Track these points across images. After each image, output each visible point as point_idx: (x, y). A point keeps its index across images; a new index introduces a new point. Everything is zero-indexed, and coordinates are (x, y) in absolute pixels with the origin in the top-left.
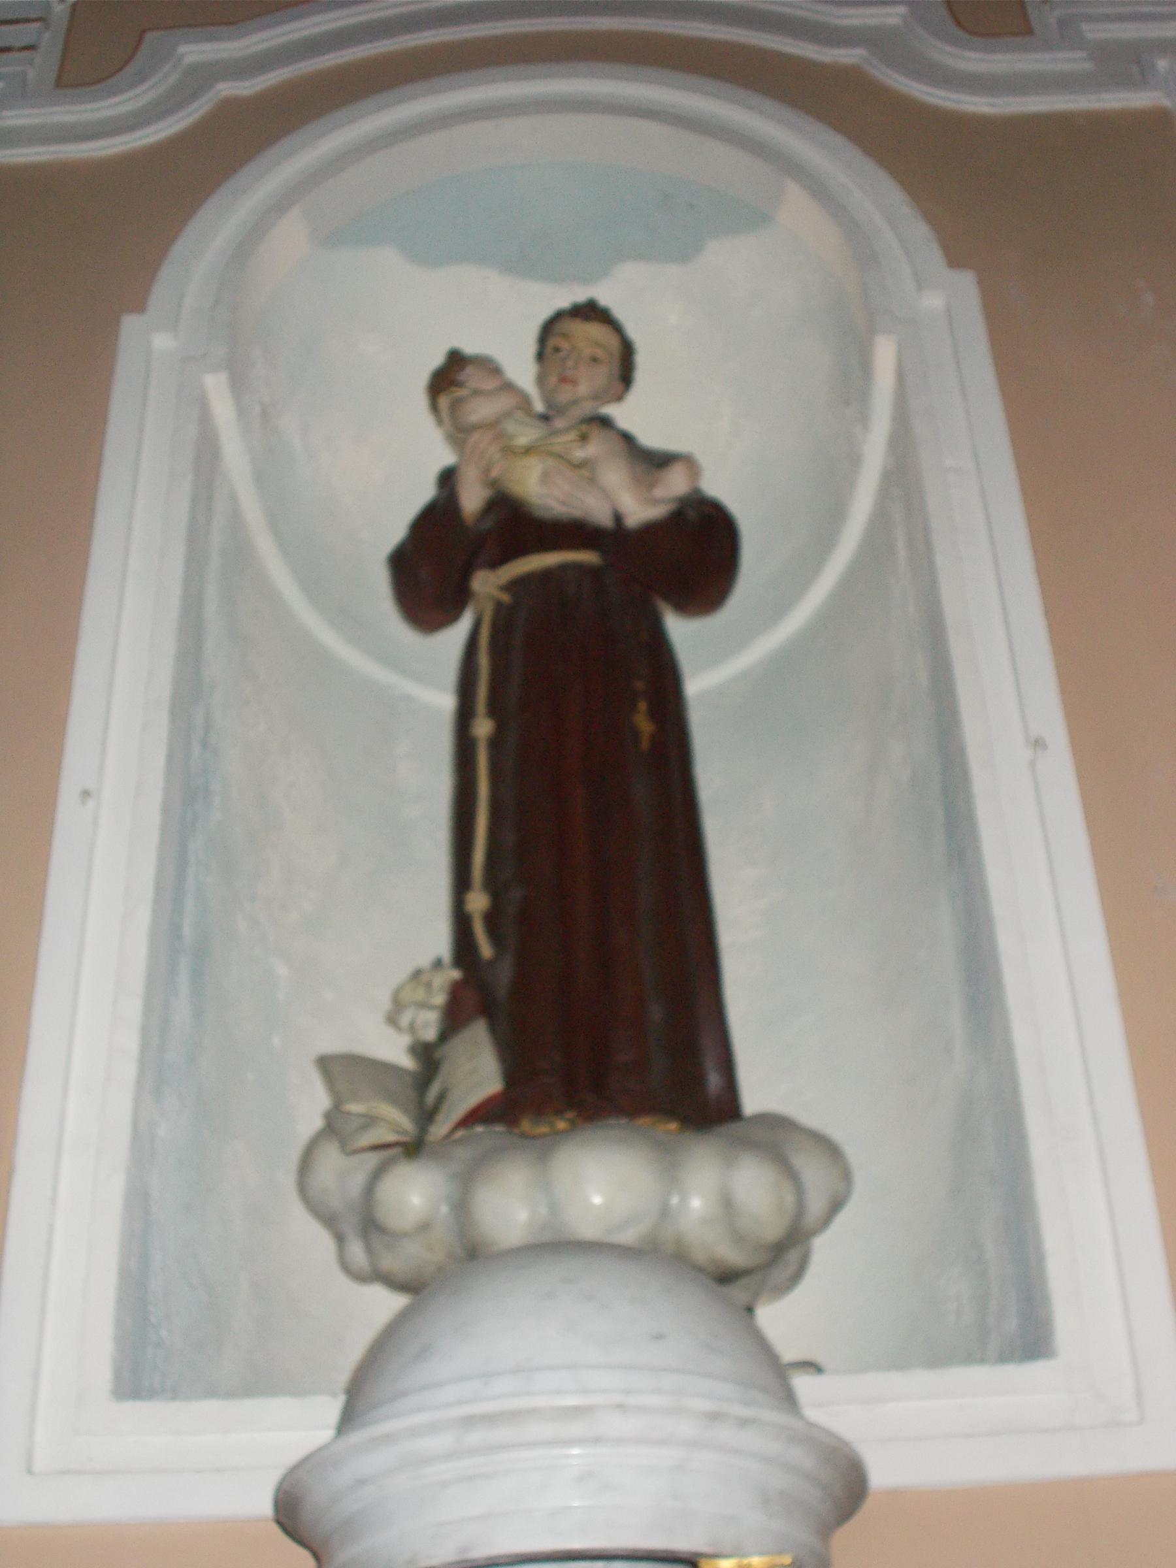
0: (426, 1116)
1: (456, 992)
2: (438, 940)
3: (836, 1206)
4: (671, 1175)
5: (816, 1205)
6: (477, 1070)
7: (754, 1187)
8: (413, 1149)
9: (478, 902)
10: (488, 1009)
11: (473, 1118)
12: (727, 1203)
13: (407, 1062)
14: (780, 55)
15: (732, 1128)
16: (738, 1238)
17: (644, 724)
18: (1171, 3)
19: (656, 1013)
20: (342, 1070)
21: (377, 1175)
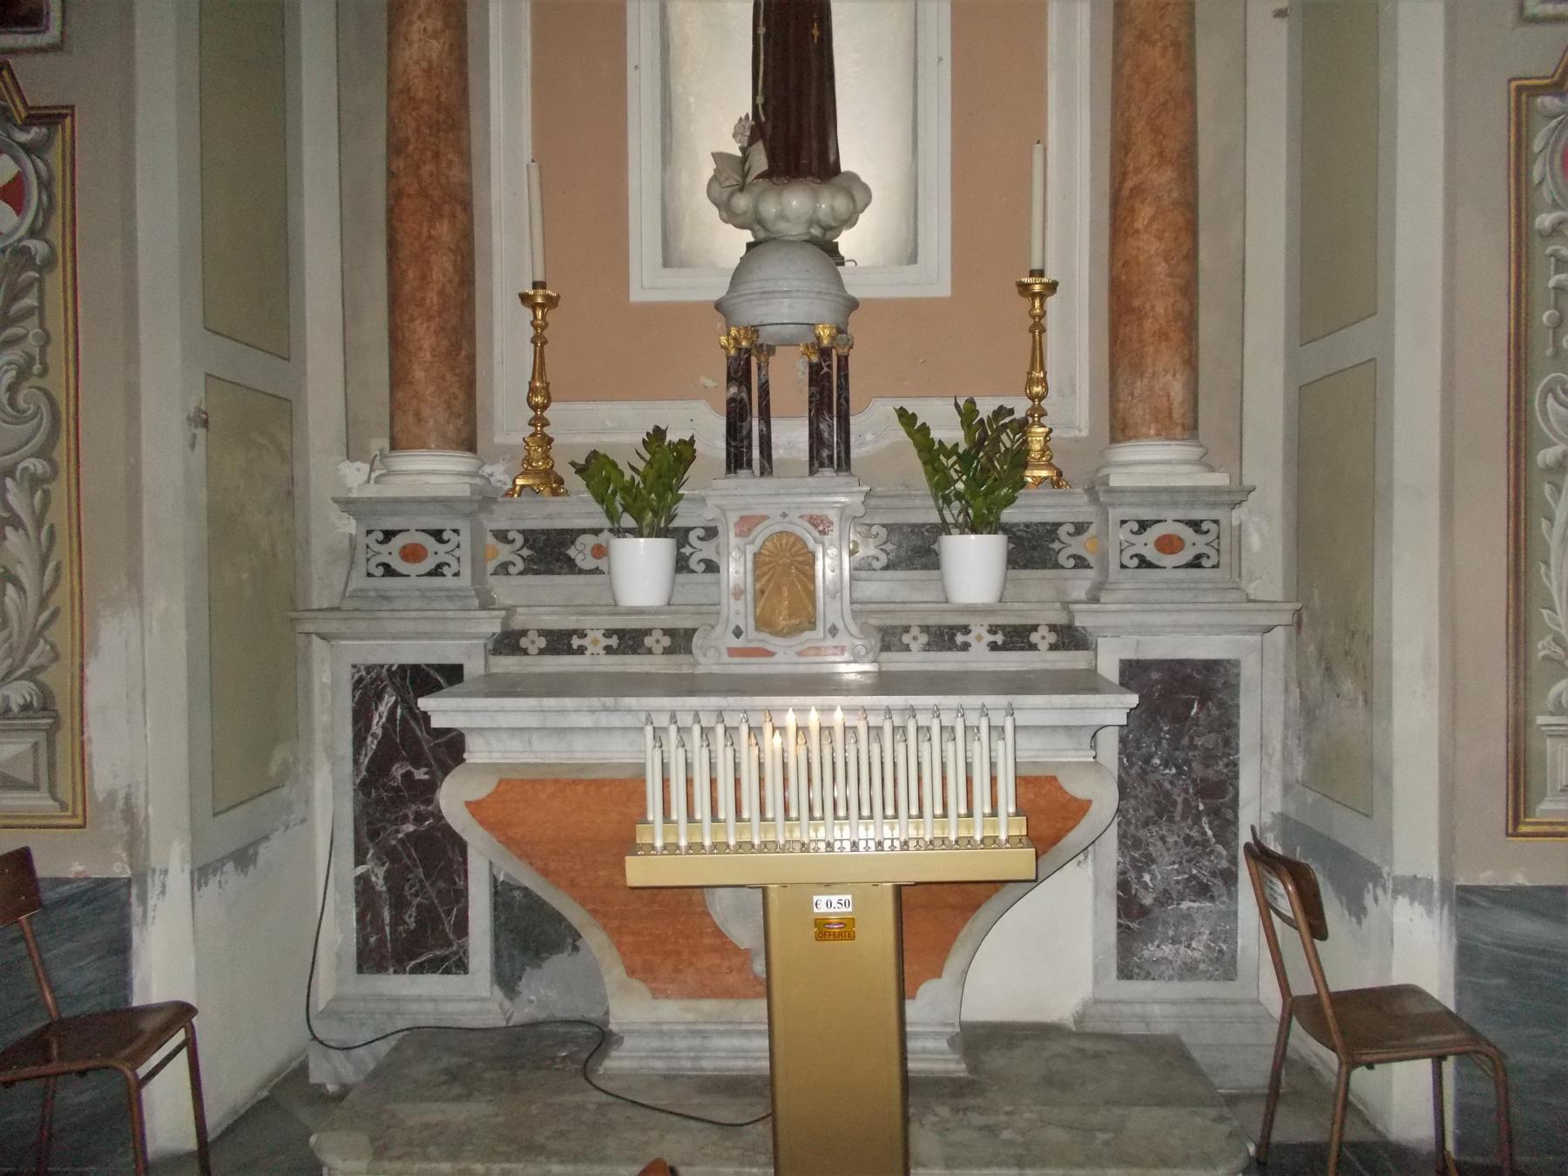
0: (745, 176)
1: (753, 129)
2: (748, 109)
3: (866, 205)
4: (816, 197)
5: (860, 204)
6: (760, 161)
7: (841, 204)
8: (741, 189)
9: (760, 100)
10: (763, 137)
11: (758, 177)
12: (833, 209)
13: (739, 154)
14: (1030, 213)
15: (836, 180)
16: (835, 219)
17: (816, 32)
18: (1564, 824)
19: (815, 145)
20: (718, 157)
21: (731, 195)
